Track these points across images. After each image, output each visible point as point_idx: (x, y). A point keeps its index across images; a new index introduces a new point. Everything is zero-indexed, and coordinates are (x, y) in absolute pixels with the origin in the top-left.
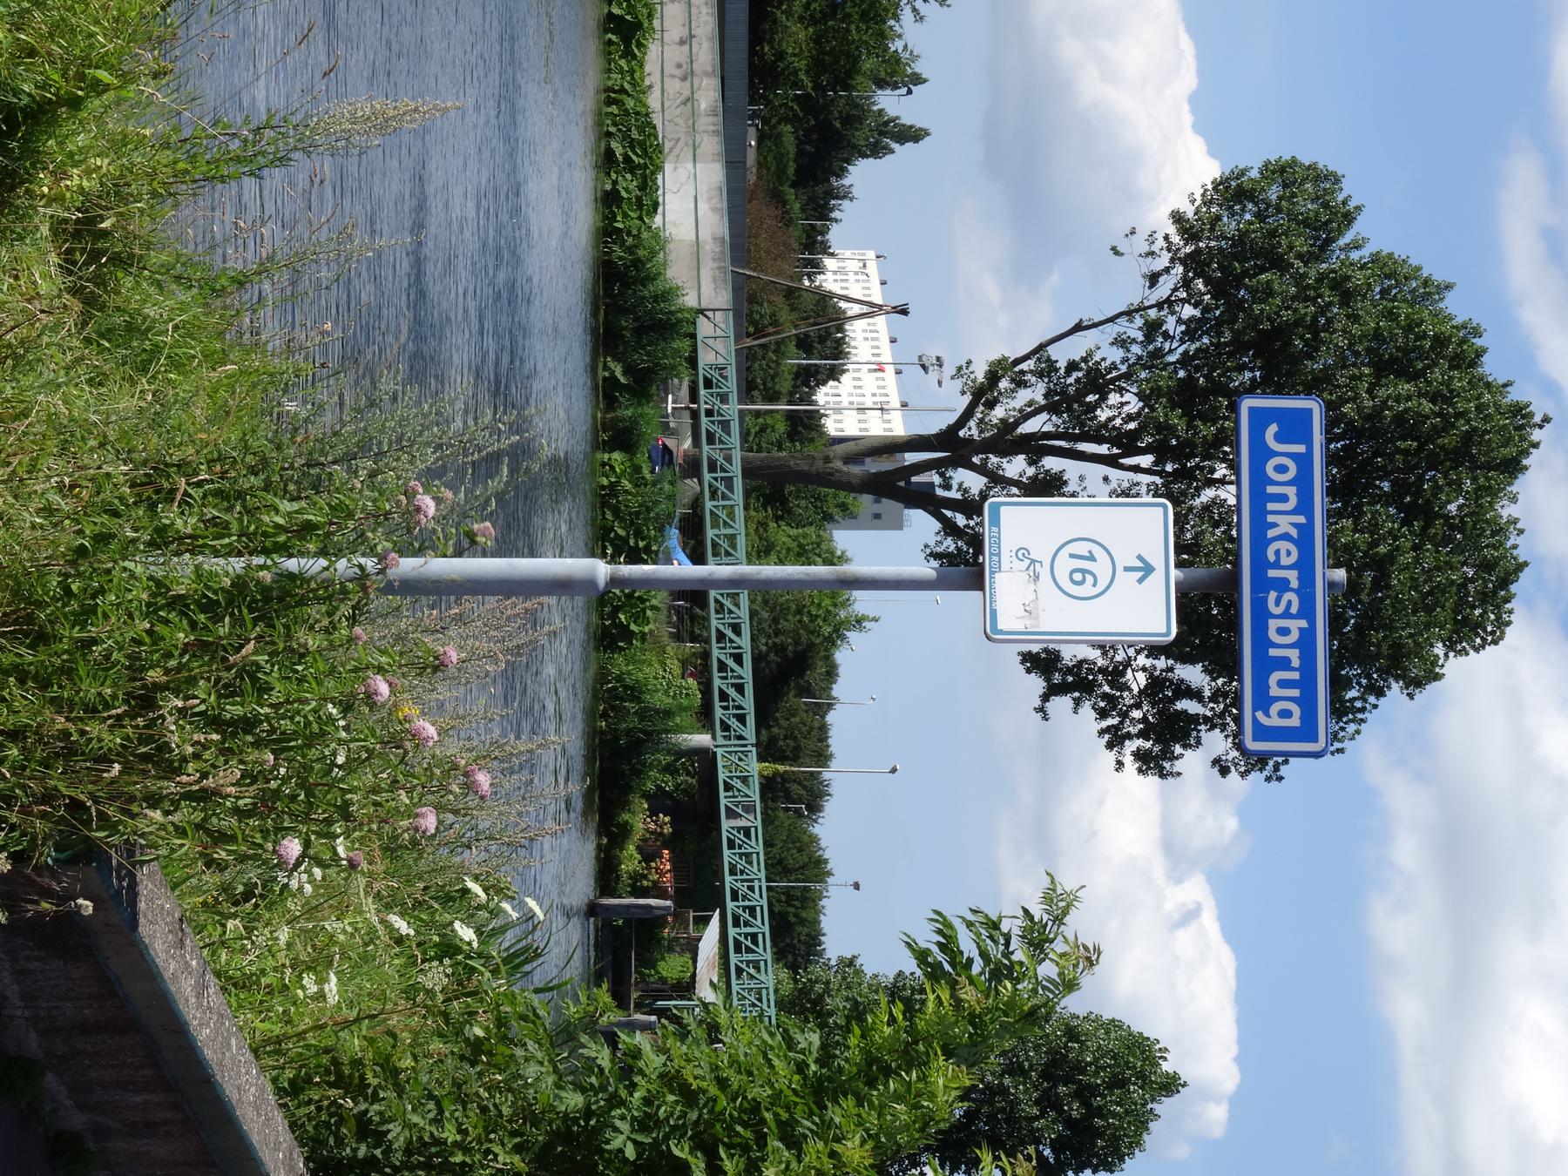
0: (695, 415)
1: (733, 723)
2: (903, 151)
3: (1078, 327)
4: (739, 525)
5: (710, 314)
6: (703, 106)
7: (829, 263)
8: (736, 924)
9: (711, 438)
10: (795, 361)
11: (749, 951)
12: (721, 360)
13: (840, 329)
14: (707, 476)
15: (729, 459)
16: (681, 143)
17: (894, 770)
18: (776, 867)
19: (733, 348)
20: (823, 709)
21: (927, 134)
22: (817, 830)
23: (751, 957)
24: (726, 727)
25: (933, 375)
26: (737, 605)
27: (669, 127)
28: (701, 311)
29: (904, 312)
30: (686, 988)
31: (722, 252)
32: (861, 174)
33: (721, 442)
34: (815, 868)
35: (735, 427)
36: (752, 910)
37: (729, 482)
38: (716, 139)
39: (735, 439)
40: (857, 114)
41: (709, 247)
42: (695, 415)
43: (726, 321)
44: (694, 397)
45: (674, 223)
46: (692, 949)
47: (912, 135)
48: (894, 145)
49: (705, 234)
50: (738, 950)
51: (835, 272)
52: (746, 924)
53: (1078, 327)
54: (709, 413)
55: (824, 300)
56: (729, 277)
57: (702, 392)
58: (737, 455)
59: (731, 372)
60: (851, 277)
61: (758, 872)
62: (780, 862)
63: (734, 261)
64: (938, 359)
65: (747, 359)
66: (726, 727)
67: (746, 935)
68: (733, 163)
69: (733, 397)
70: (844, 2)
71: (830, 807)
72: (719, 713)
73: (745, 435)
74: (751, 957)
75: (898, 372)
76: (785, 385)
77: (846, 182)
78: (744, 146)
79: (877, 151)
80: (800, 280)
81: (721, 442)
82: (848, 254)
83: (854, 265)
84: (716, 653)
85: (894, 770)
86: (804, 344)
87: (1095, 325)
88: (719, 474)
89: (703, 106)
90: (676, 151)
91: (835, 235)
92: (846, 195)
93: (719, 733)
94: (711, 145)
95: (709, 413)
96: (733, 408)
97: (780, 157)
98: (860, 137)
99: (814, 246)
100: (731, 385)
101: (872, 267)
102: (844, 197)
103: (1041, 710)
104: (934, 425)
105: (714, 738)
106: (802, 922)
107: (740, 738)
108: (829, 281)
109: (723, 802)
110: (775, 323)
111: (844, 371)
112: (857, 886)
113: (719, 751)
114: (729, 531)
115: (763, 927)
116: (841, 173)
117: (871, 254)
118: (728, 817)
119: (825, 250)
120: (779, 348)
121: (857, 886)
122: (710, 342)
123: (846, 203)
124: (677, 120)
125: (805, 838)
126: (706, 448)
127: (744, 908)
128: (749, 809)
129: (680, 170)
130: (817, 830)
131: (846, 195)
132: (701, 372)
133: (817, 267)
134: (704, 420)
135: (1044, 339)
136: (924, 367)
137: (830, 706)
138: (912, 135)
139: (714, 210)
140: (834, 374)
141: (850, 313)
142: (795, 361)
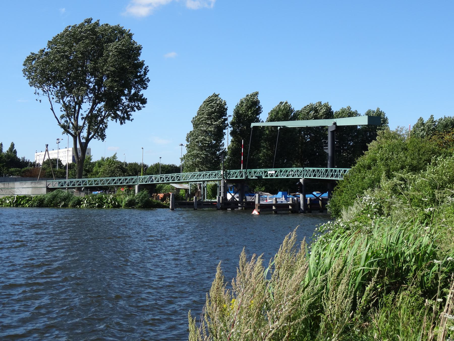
0: (69, 188)
1: (127, 181)
2: (16, 148)
3: (52, 109)
4: (92, 179)
5: (47, 185)
6: (3, 186)
7: (37, 162)
8: (163, 181)
9: (74, 185)
10: (57, 168)
11: (169, 178)
12: (57, 183)
13: (51, 160)
14: (82, 186)
15: (78, 181)
16: (11, 191)
17: (143, 148)
18: (157, 173)
19: (55, 180)
20: (126, 164)
21: (12, 143)
22: (149, 166)
23: (170, 178)
24: (134, 182)
25: (60, 140)
26: (103, 180)
27: (7, 193)
28: (47, 187)
29: (47, 145)
30: (186, 190)
31: (34, 182)
32: (20, 156)
33: (75, 183)
34: (157, 165)
35: (71, 180)
36: (166, 177)
37: (83, 181)
38: (10, 184)
39: (74, 180)
40: (8, 156)
41: (33, 185)
42: (69, 188)
43: (49, 182)
44: (65, 188)
45: (28, 192)
46: (178, 190)
47: (13, 145)
48: (14, 149)
49: (30, 186)
50: (174, 180)
51: (39, 161)
52: (164, 179)
53: (52, 109)
54: (68, 185)
55: (44, 163)
56: (40, 181)
57: (64, 187)
58: (77, 180)
59: (60, 181)
60: (40, 158)
61: (159, 176)
62: (156, 172)
63: (36, 180)
64: (57, 140)
65: (58, 177)
66: (134, 182)
67: (166, 179)
68: (15, 180)
69: (65, 180)
70: (379, 338)
71: (146, 163)
72: (131, 184)
73: (73, 178)
74: (170, 178)
75: (60, 149)
76: (63, 171)
77: (21, 158)
78: (12, 178)
79: (15, 152)
80: (40, 168)
81: (75, 183)
82: (36, 159)
83: (38, 157)
84: (119, 184)
85: (143, 148)
86: (54, 167)
87: (52, 106)
88: (93, 183)
89: (3, 186)
90: (12, 192)
91: (32, 161)
92: (24, 158)
93: (135, 184)
94: (11, 185)
95: (68, 185)
96: (68, 181)
97: (16, 171)
98: (12, 155)
99: (34, 165)
100: (63, 181)
101: (38, 154)
102: (24, 159)
103: (132, 120)
104: (71, 139)
105: (301, 178)
106: (167, 168)
107: (136, 180)
108: (41, 162)
109: (149, 183)
110: (50, 172)
111: (59, 159)
112: (161, 158)
113: (139, 184)
114: (93, 181)
115: (170, 175)
116: (19, 159)
117: (36, 154)
118: (242, 177)
119: (35, 163)
120: (54, 171)
121: (161, 158)
122: (53, 185)
123: (25, 159)
124: (6, 192)
125: (151, 167)
126: (76, 186)
127: (161, 179)
128: (151, 178)
129: (16, 191)
130: (149, 166)
131: (24, 158)
132: (60, 187)
133: (38, 165)
134: (70, 186)
135: (54, 116)
136: (59, 143)
137: (126, 163)
138: (13, 145)
139: (25, 184)
140: (60, 161)
141: (48, 158)
142: (57, 168)
